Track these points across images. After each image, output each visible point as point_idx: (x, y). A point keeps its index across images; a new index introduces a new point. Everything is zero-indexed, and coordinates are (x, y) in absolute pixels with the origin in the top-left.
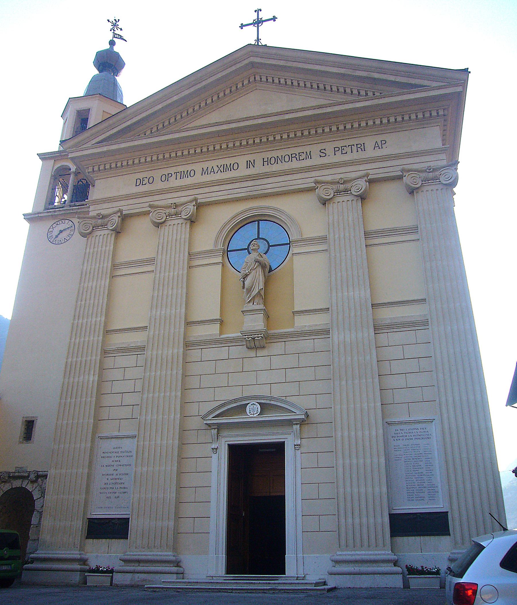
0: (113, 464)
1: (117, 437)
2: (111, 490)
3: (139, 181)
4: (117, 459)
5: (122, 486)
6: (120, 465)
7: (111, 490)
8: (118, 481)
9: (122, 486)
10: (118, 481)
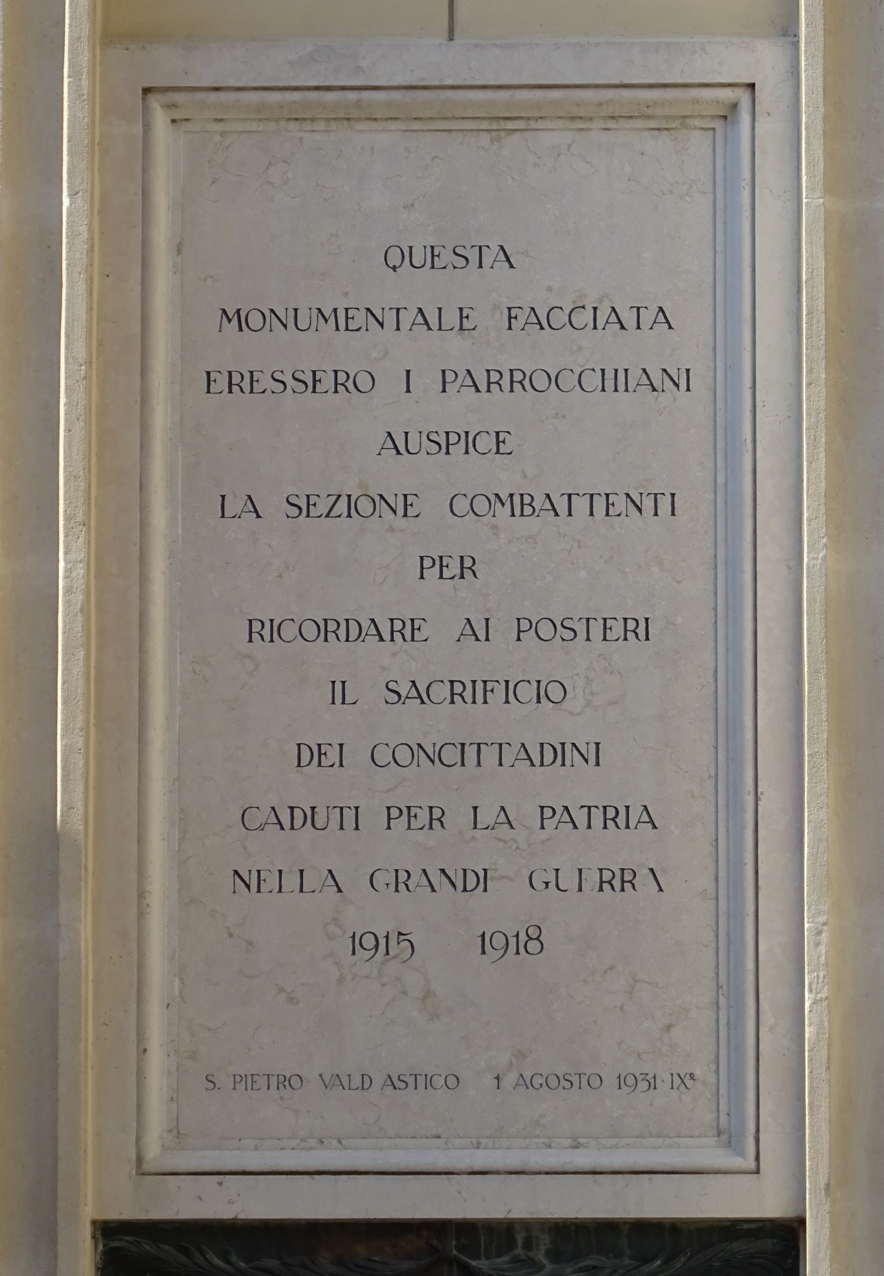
0: (394, 476)
1: (425, 108)
2: (404, 848)
3: (548, 751)
4: (460, 411)
5: (576, 786)
6: (519, 504)
7: (404, 848)
8: (492, 721)
9: (576, 786)
10: (492, 721)
